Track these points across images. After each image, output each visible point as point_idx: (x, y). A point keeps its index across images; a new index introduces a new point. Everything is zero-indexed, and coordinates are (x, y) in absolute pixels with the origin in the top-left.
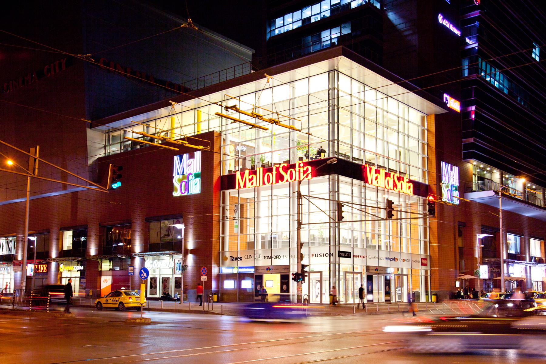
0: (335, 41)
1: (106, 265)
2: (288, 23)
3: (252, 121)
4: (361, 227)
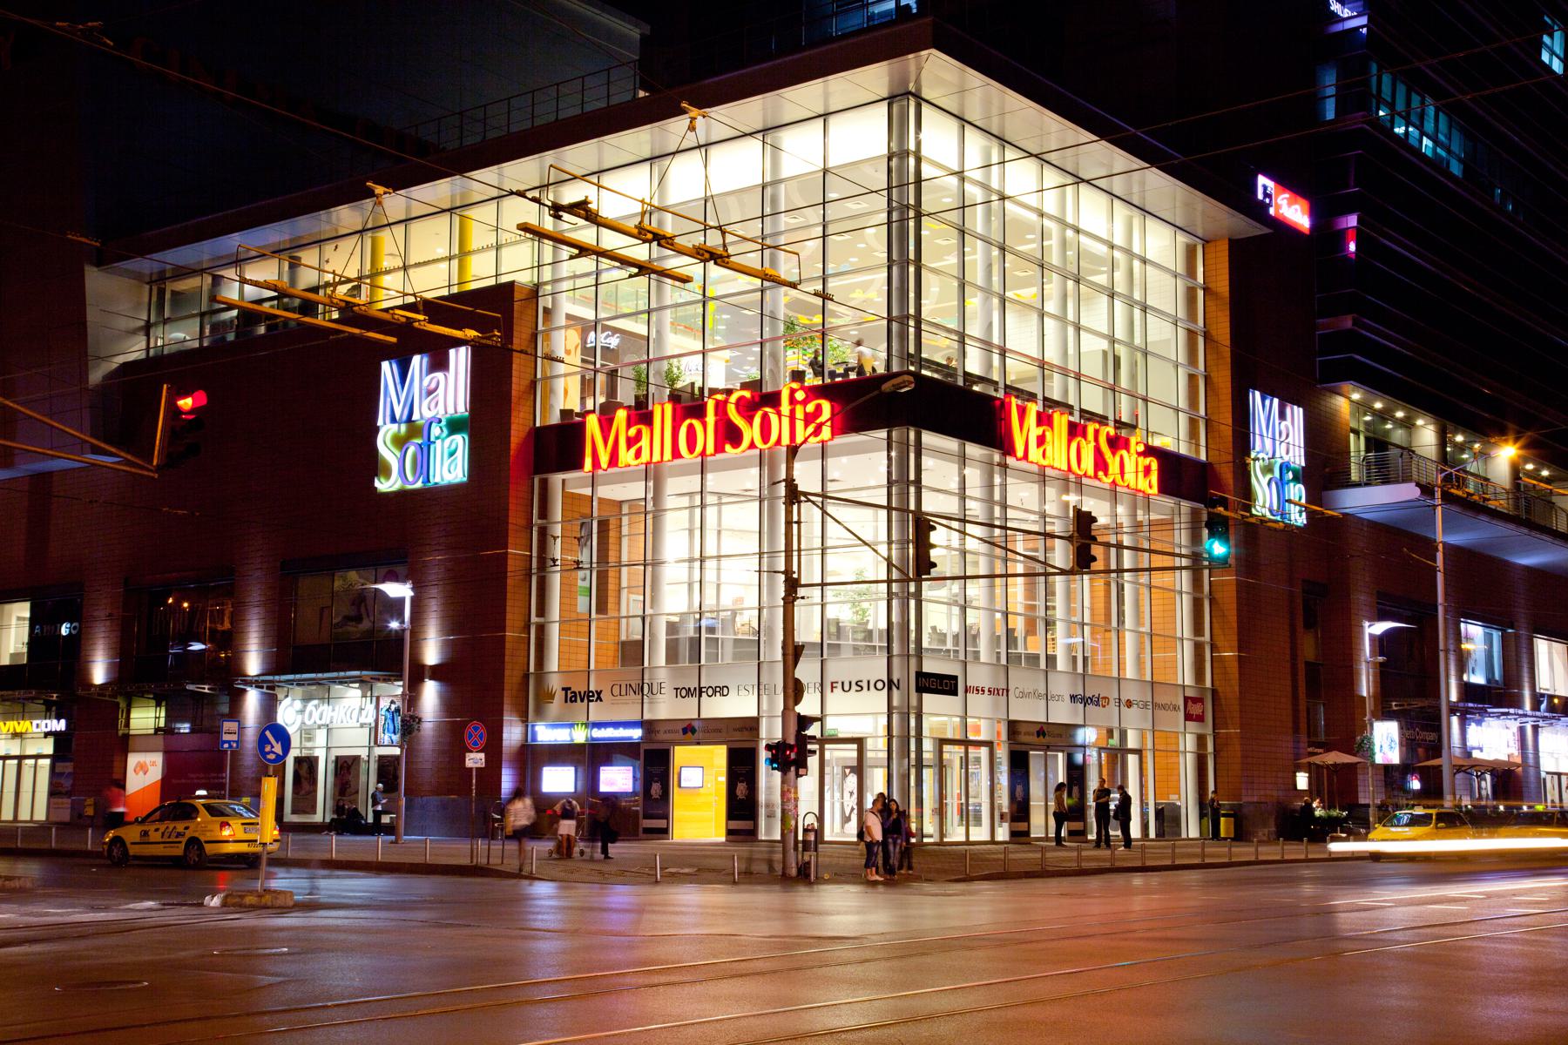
1: (145, 718)
3: (641, 252)
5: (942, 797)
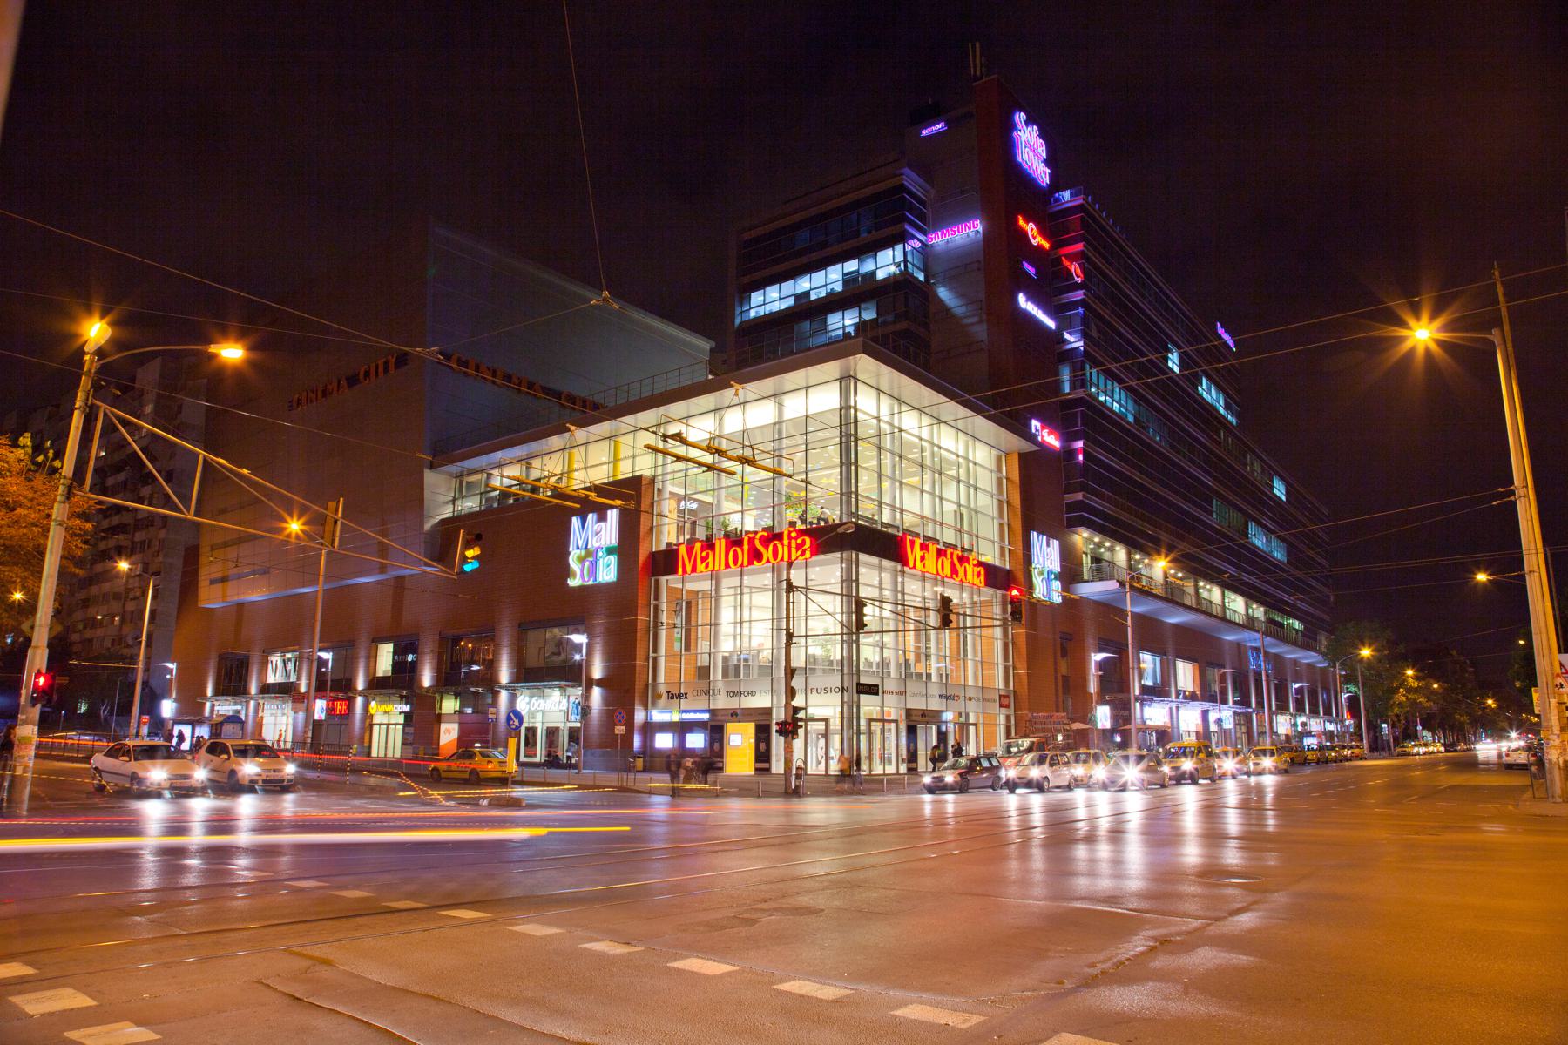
0: (851, 330)
1: (449, 705)
2: (771, 300)
3: (709, 459)
4: (897, 642)
5: (870, 750)
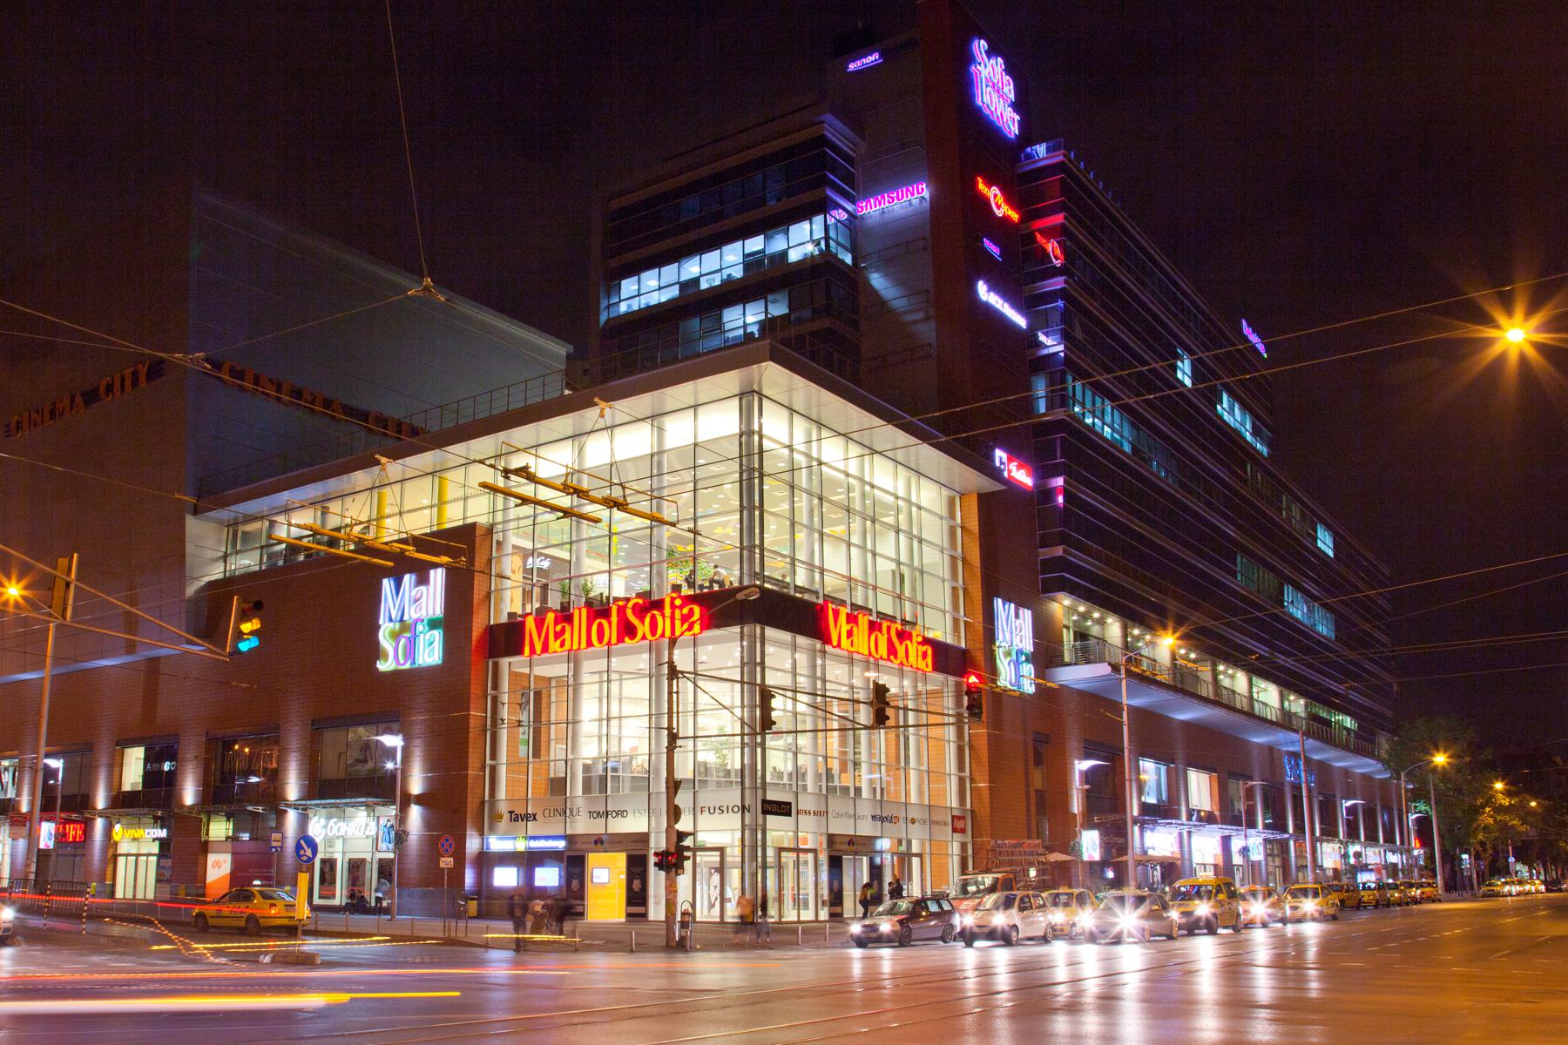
0: (754, 329)
